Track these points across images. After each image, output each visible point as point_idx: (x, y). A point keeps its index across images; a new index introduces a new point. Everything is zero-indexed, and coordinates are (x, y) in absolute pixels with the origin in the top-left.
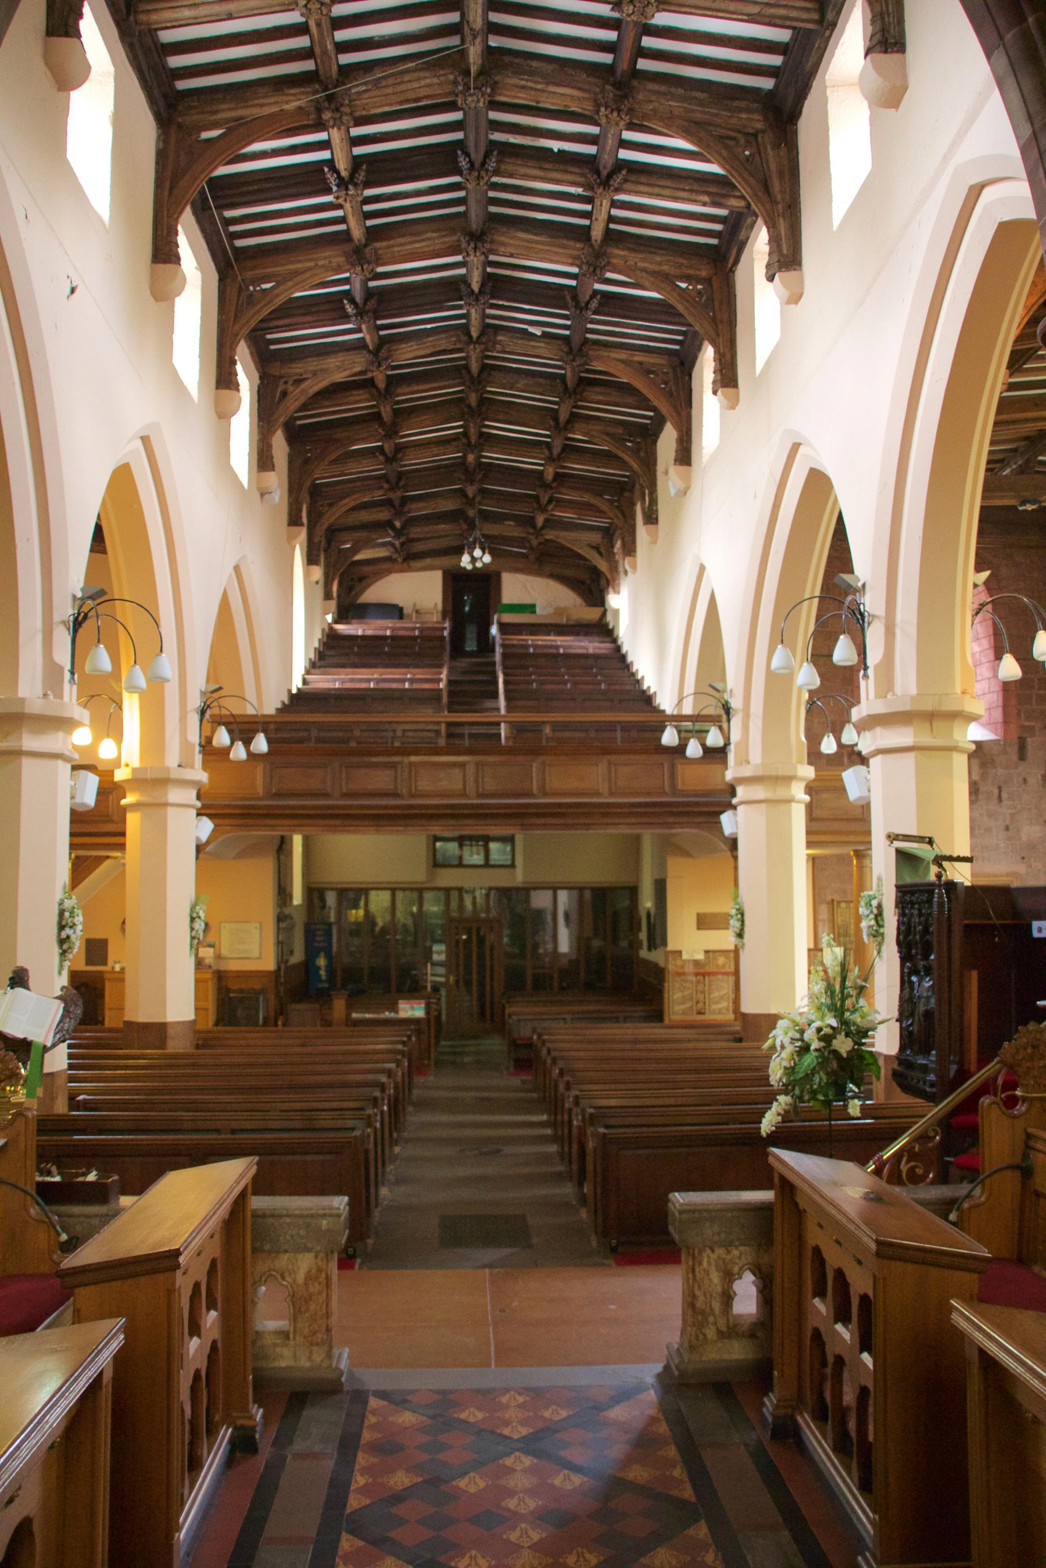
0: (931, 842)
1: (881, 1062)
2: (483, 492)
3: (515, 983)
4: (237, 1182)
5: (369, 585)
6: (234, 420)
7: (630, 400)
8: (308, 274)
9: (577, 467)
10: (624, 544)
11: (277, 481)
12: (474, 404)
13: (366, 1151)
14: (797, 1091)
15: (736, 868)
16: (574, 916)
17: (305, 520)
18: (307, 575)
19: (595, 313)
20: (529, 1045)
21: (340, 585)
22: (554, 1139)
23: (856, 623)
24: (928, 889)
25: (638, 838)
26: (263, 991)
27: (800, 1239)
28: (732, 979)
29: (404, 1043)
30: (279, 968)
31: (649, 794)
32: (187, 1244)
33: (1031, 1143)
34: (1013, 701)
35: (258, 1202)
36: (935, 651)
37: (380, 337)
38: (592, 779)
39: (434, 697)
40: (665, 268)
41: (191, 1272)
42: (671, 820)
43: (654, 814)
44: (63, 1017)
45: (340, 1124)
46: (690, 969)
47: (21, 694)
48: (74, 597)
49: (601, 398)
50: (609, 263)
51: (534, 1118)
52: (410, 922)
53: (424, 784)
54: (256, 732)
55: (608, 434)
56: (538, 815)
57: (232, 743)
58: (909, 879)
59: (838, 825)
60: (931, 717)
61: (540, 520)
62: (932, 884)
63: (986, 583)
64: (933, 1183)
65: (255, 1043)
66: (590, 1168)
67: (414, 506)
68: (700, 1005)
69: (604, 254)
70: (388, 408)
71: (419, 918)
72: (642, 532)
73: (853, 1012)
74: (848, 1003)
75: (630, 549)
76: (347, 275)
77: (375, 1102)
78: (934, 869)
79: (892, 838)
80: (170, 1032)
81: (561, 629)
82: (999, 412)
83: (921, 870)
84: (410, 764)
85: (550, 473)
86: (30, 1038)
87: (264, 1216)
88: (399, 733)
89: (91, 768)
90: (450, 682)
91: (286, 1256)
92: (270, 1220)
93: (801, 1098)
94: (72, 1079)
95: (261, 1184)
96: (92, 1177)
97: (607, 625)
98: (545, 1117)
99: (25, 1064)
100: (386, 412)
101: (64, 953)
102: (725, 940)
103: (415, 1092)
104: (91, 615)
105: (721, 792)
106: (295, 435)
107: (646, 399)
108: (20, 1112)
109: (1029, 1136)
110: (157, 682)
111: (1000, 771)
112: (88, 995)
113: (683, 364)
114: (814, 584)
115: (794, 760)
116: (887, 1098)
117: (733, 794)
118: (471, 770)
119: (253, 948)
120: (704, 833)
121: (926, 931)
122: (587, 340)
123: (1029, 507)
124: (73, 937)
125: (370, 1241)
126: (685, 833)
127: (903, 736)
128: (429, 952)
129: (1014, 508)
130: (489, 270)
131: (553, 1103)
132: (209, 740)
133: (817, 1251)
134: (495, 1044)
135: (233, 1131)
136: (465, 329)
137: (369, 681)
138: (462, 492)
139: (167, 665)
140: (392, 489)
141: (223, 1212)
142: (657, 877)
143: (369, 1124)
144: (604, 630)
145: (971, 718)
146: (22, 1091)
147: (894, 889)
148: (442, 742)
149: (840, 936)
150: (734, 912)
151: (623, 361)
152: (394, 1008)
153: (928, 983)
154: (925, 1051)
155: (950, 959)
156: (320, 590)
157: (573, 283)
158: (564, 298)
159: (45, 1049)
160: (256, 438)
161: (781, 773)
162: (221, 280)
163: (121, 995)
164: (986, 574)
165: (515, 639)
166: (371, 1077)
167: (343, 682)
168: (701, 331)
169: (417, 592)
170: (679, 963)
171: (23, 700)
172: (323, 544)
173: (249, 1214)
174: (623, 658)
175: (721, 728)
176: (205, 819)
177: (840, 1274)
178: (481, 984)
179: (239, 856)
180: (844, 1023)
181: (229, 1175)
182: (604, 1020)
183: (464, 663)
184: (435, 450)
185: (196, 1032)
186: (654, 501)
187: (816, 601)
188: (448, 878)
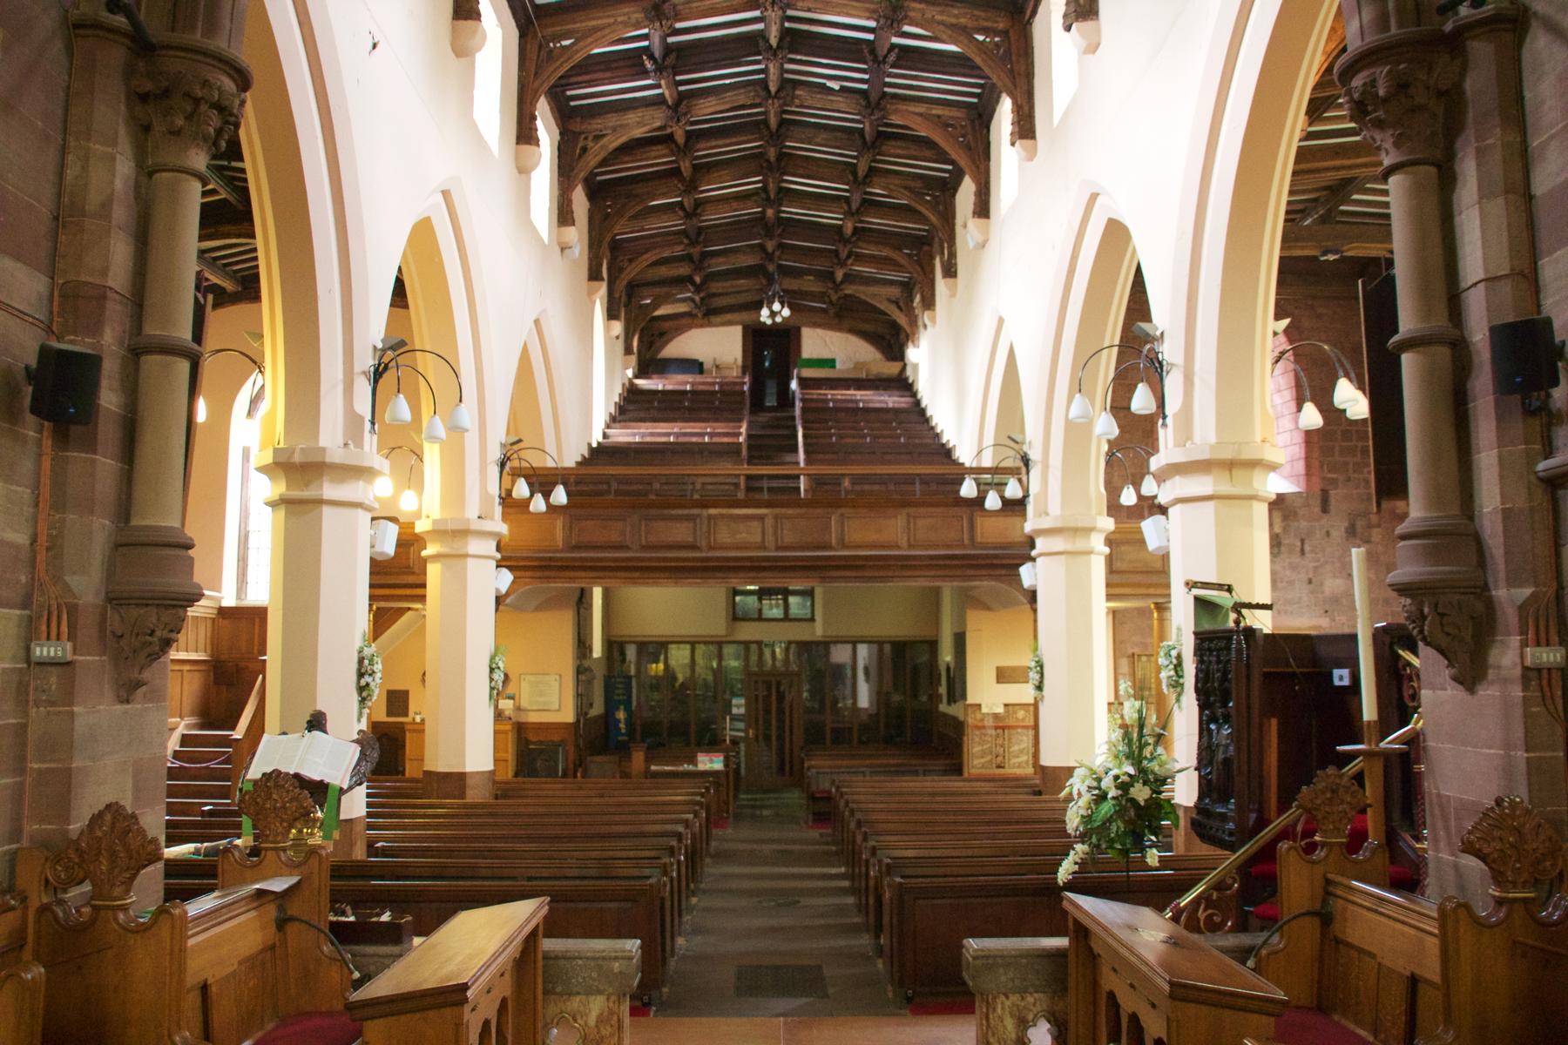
0: (1229, 589)
1: (1181, 813)
2: (781, 246)
3: (815, 738)
4: (528, 921)
5: (670, 340)
6: (534, 174)
7: (928, 153)
8: (607, 31)
9: (876, 221)
10: (923, 299)
11: (577, 235)
12: (772, 159)
13: (663, 899)
14: (1094, 840)
15: (1035, 621)
16: (873, 672)
17: (605, 275)
18: (607, 330)
19: (893, 66)
20: (828, 798)
21: (640, 340)
22: (852, 891)
23: (1155, 372)
24: (1227, 635)
25: (936, 593)
26: (562, 743)
27: (1095, 984)
28: (1031, 732)
29: (702, 795)
30: (578, 721)
31: (948, 546)
32: (476, 978)
33: (1331, 889)
34: (1316, 454)
35: (549, 945)
36: (1243, 412)
37: (680, 93)
38: (891, 531)
39: (731, 451)
40: (963, 20)
41: (480, 1011)
42: (971, 572)
43: (950, 567)
44: (359, 760)
45: (635, 872)
46: (989, 722)
47: (322, 443)
48: (375, 348)
49: (899, 151)
50: (906, 17)
51: (834, 871)
52: (710, 678)
53: (724, 535)
54: (555, 484)
55: (906, 188)
56: (838, 568)
57: (532, 495)
58: (1207, 626)
59: (1136, 576)
60: (1230, 465)
61: (839, 275)
62: (1231, 631)
63: (1286, 331)
64: (1233, 930)
65: (554, 793)
66: (886, 920)
67: (714, 261)
68: (1000, 759)
69: (902, 7)
70: (687, 164)
71: (719, 673)
72: (941, 285)
73: (1151, 760)
74: (1147, 752)
75: (929, 303)
76: (646, 31)
77: (672, 852)
78: (1233, 616)
79: (1191, 585)
80: (469, 782)
81: (860, 384)
82: (1297, 162)
83: (1220, 618)
84: (710, 517)
85: (849, 228)
86: (327, 780)
87: (556, 958)
88: (698, 486)
89: (393, 520)
90: (750, 437)
91: (578, 998)
92: (562, 962)
93: (1098, 846)
94: (370, 827)
95: (553, 926)
96: (386, 917)
97: (906, 379)
98: (843, 870)
99: (321, 807)
100: (686, 167)
101: (363, 701)
102: (1023, 693)
103: (713, 844)
104: (391, 365)
105: (1021, 544)
106: (596, 192)
107: (946, 153)
108: (314, 851)
109: (1328, 882)
110: (456, 430)
111: (1304, 524)
112: (387, 749)
113: (982, 116)
114: (1113, 332)
115: (1094, 512)
116: (1187, 849)
117: (1033, 546)
118: (769, 522)
119: (553, 701)
120: (1005, 587)
121: (1224, 678)
122: (885, 94)
123: (1331, 257)
124: (372, 685)
125: (665, 990)
126: (984, 585)
127: (1202, 485)
128: (729, 705)
129: (1315, 258)
130: (787, 25)
131: (850, 855)
132: (509, 493)
133: (1112, 996)
134: (794, 797)
135: (530, 879)
136: (764, 84)
137: (669, 435)
138: (762, 247)
139: (467, 415)
140: (692, 244)
141: (514, 949)
142: (958, 630)
143: (665, 873)
144: (903, 384)
145: (1272, 467)
146: (319, 833)
147: (1192, 637)
148: (741, 495)
149: (1140, 691)
150: (1033, 664)
151: (921, 115)
152: (693, 761)
153: (1226, 731)
154: (1224, 800)
155: (1249, 707)
156: (620, 345)
157: (871, 37)
158: (861, 51)
159: (342, 791)
160: (556, 193)
161: (1080, 525)
162: (523, 35)
163: (421, 747)
164: (1286, 322)
165: (815, 393)
166: (669, 827)
167: (643, 435)
168: (999, 84)
169: (718, 346)
170: (978, 716)
171: (324, 450)
172: (624, 299)
173: (540, 956)
174: (922, 412)
175: (1020, 480)
176: (505, 570)
177: (1134, 1018)
178: (780, 738)
179: (538, 609)
180: (1142, 771)
181: (521, 914)
182: (903, 773)
183: (763, 418)
184: (735, 205)
185: (495, 782)
186: (953, 255)
187: (1115, 350)
188: (747, 632)
